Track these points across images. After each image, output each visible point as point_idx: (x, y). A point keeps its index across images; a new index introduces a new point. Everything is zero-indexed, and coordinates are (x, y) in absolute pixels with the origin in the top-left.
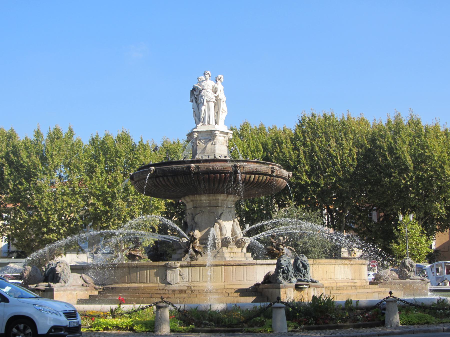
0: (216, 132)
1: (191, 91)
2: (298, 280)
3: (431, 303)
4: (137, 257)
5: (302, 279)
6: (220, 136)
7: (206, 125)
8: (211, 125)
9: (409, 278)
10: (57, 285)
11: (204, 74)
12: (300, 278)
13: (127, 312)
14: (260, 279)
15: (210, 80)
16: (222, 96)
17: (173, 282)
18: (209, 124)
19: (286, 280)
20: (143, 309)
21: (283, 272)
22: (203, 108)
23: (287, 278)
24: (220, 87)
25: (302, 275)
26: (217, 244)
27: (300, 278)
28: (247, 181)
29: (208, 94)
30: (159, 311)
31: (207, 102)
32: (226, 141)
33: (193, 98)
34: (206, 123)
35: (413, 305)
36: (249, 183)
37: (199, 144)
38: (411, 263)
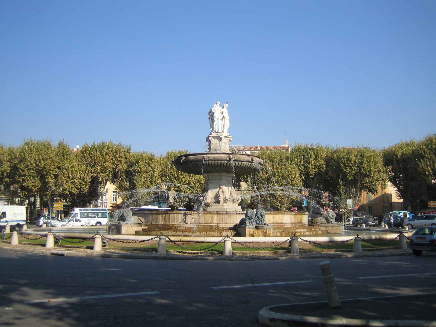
0: (222, 137)
1: (209, 113)
2: (257, 224)
3: (316, 241)
4: (175, 207)
5: (260, 223)
6: (225, 139)
9: (331, 223)
10: (124, 222)
11: (216, 103)
12: (259, 222)
13: (260, 229)
14: (238, 222)
15: (219, 106)
16: (227, 117)
17: (189, 223)
19: (251, 223)
20: (152, 239)
21: (249, 219)
22: (215, 123)
23: (251, 223)
24: (225, 111)
25: (260, 221)
26: (220, 201)
27: (259, 222)
28: (237, 165)
29: (217, 115)
30: (160, 241)
32: (228, 142)
34: (46, 210)
35: (308, 242)
36: (238, 167)
38: (332, 214)
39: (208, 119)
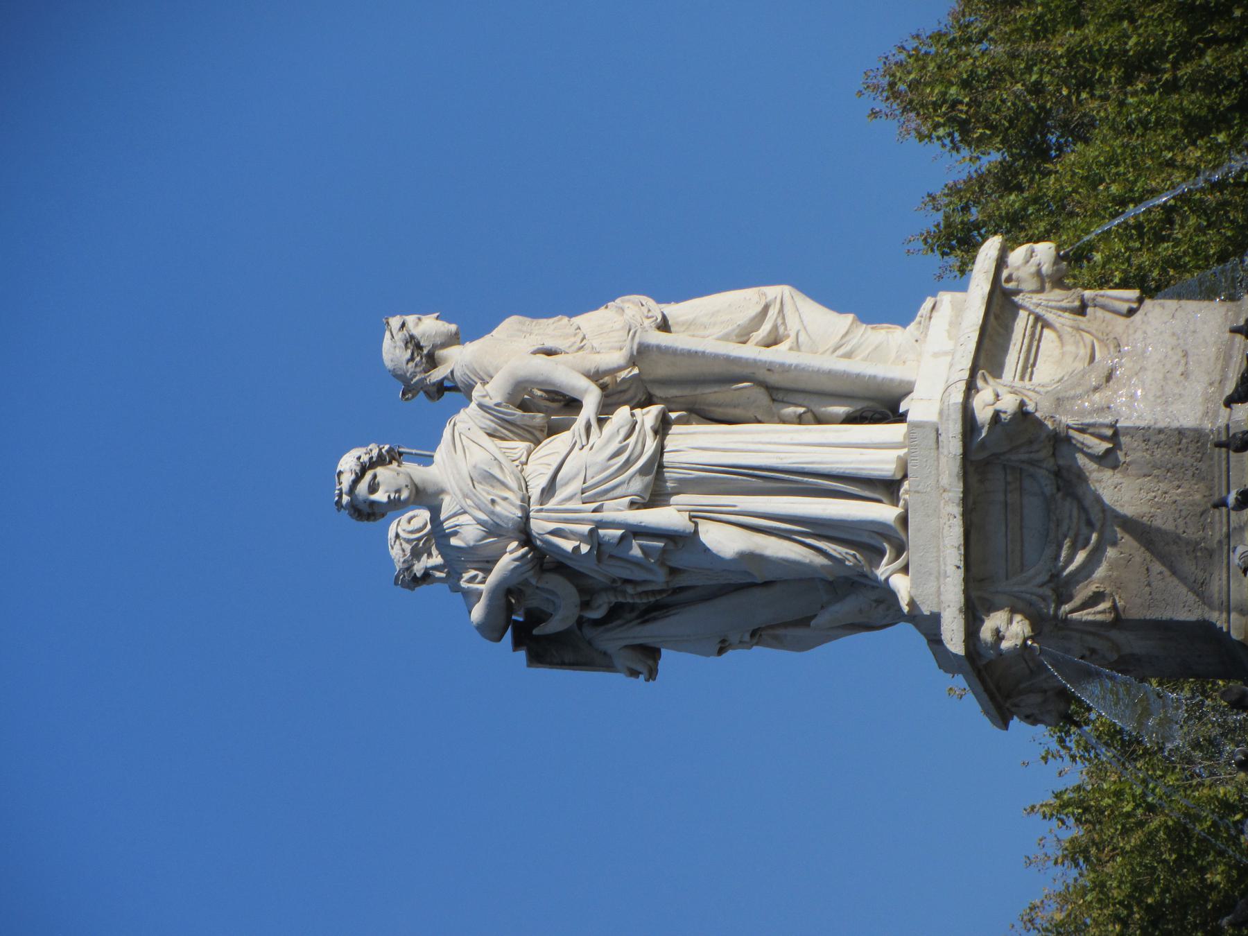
0: (983, 414)
7: (904, 520)
8: (904, 465)
18: (888, 488)
31: (656, 496)
33: (613, 640)
37: (1097, 598)
39: (652, 674)
